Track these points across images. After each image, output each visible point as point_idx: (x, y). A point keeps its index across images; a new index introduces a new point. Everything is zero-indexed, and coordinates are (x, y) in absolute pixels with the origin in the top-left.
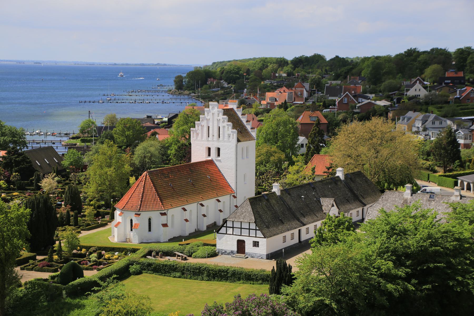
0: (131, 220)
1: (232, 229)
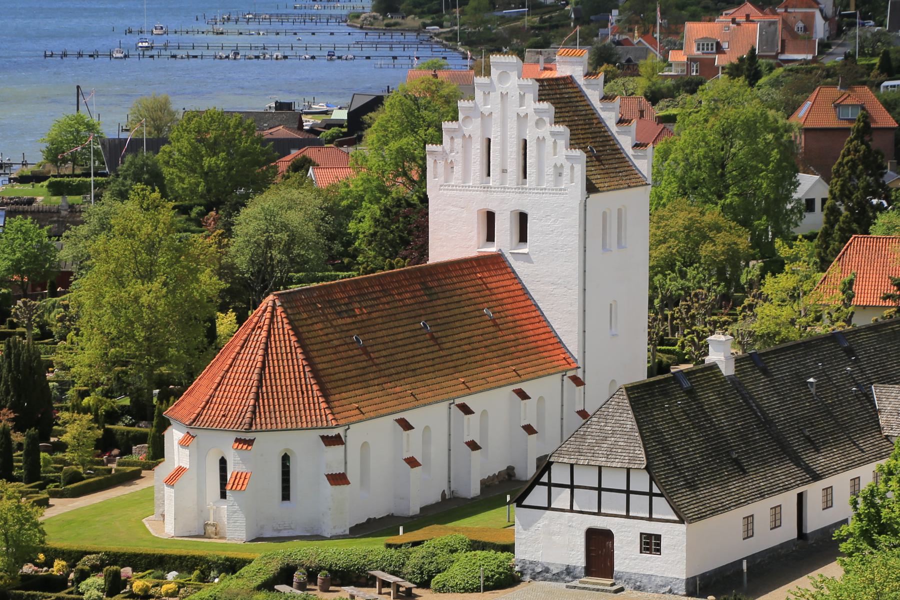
0: (223, 462)
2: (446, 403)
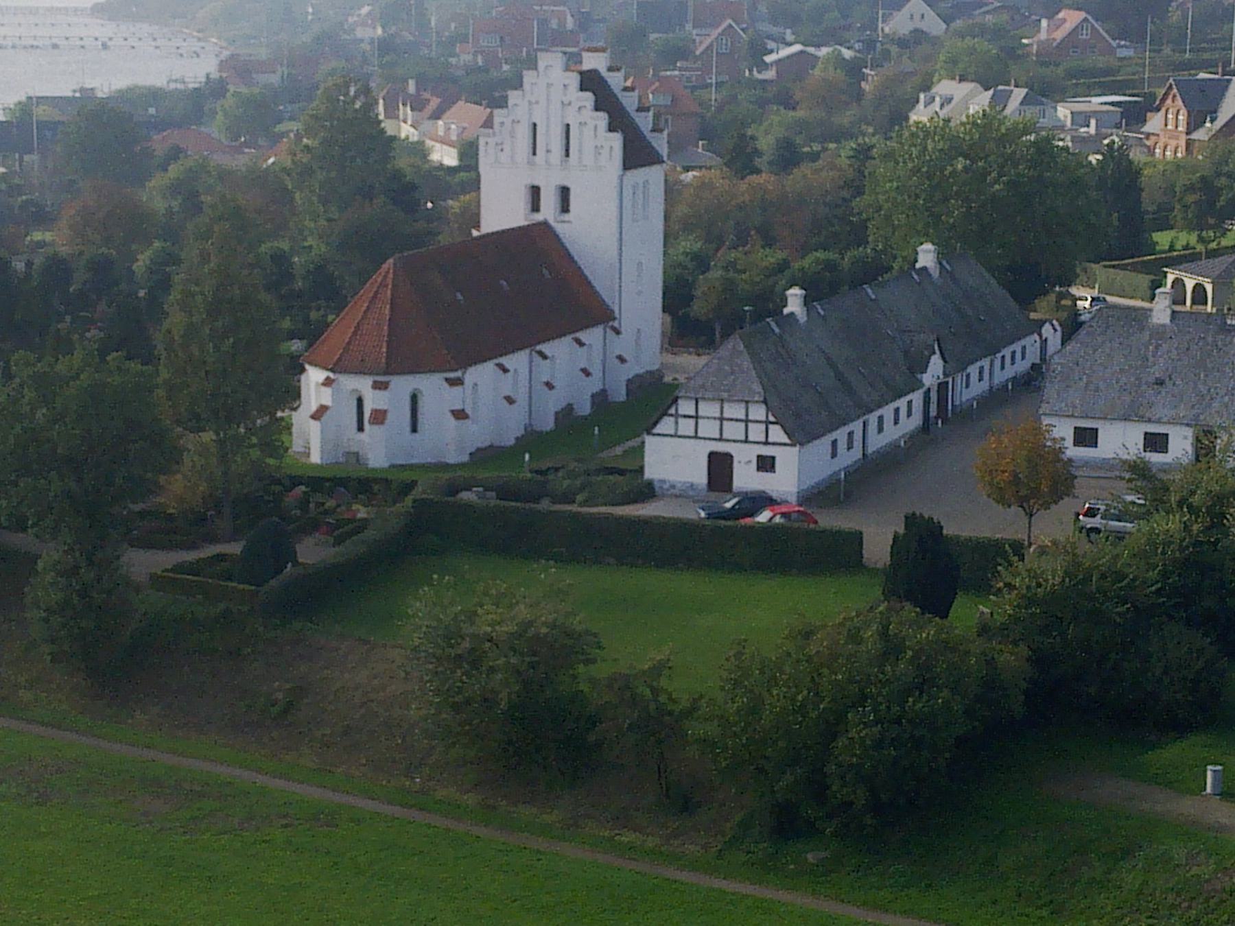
0: (360, 401)
1: (725, 423)
2: (527, 351)
